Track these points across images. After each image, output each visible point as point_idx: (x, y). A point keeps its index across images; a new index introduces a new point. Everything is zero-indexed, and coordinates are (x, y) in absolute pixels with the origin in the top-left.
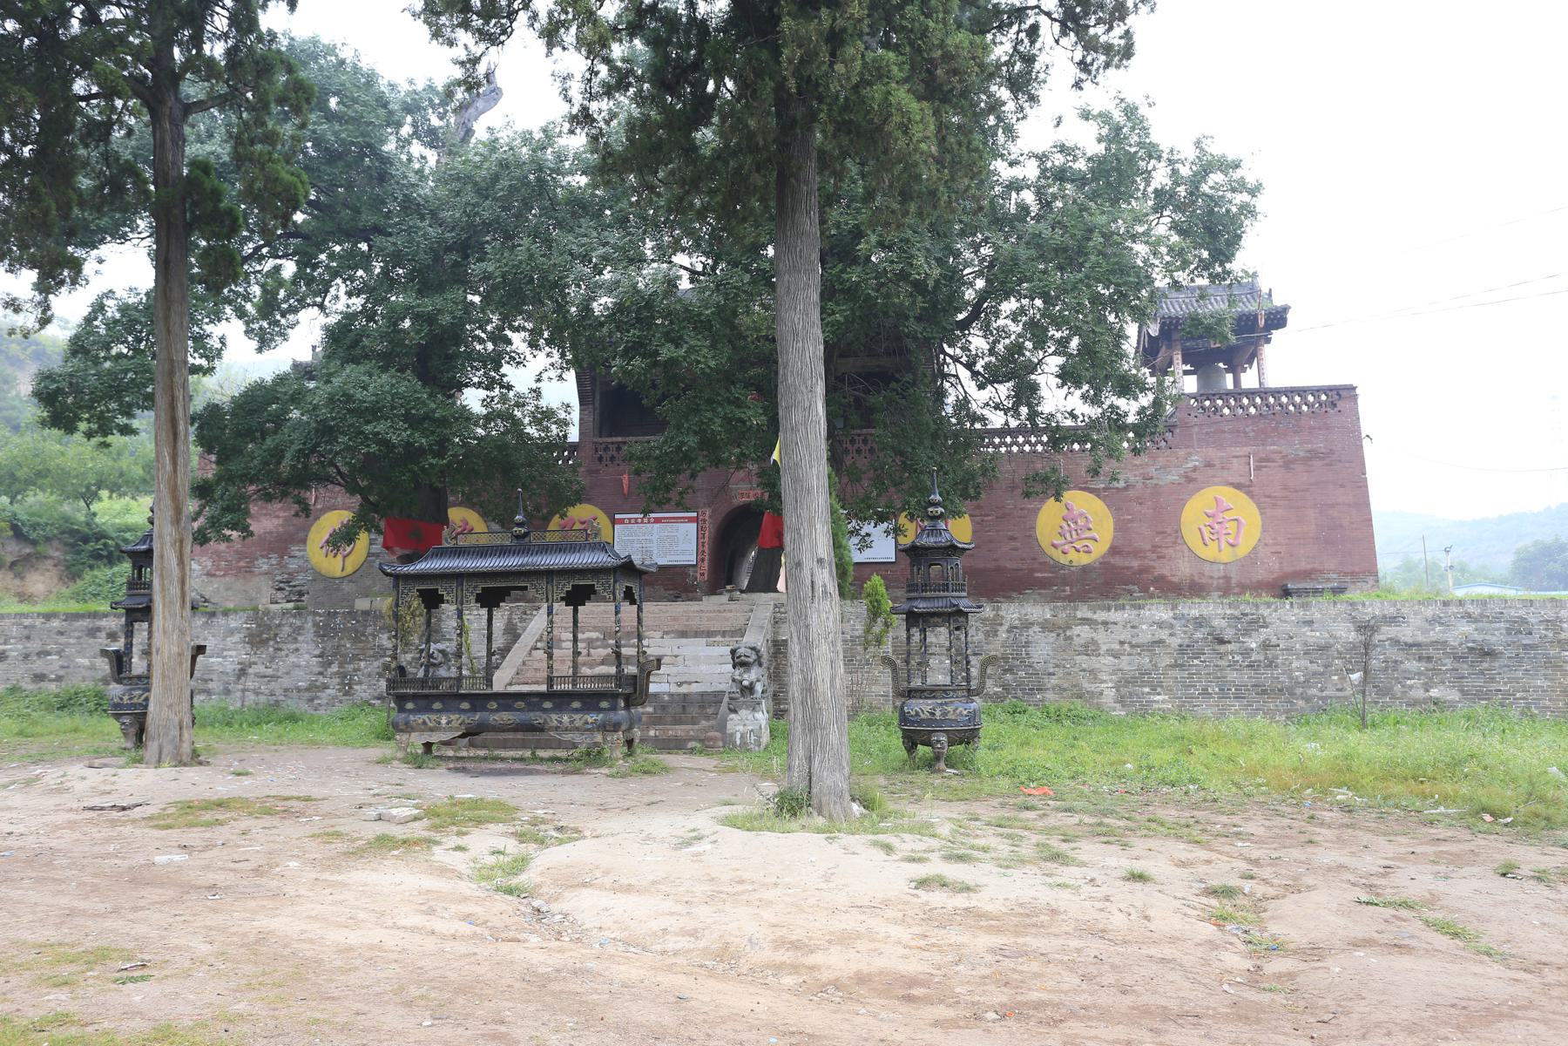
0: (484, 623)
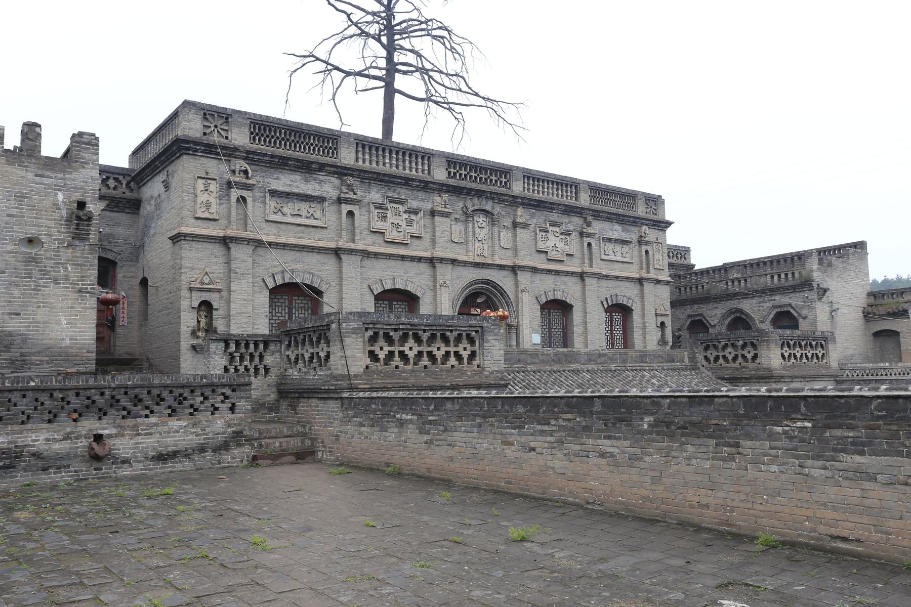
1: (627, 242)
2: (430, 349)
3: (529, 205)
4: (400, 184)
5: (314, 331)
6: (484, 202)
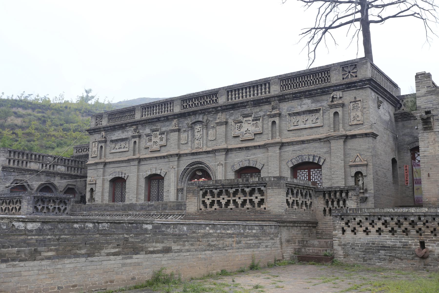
1: (316, 110)
2: (218, 199)
3: (227, 109)
4: (156, 121)
5: (295, 188)
6: (197, 117)
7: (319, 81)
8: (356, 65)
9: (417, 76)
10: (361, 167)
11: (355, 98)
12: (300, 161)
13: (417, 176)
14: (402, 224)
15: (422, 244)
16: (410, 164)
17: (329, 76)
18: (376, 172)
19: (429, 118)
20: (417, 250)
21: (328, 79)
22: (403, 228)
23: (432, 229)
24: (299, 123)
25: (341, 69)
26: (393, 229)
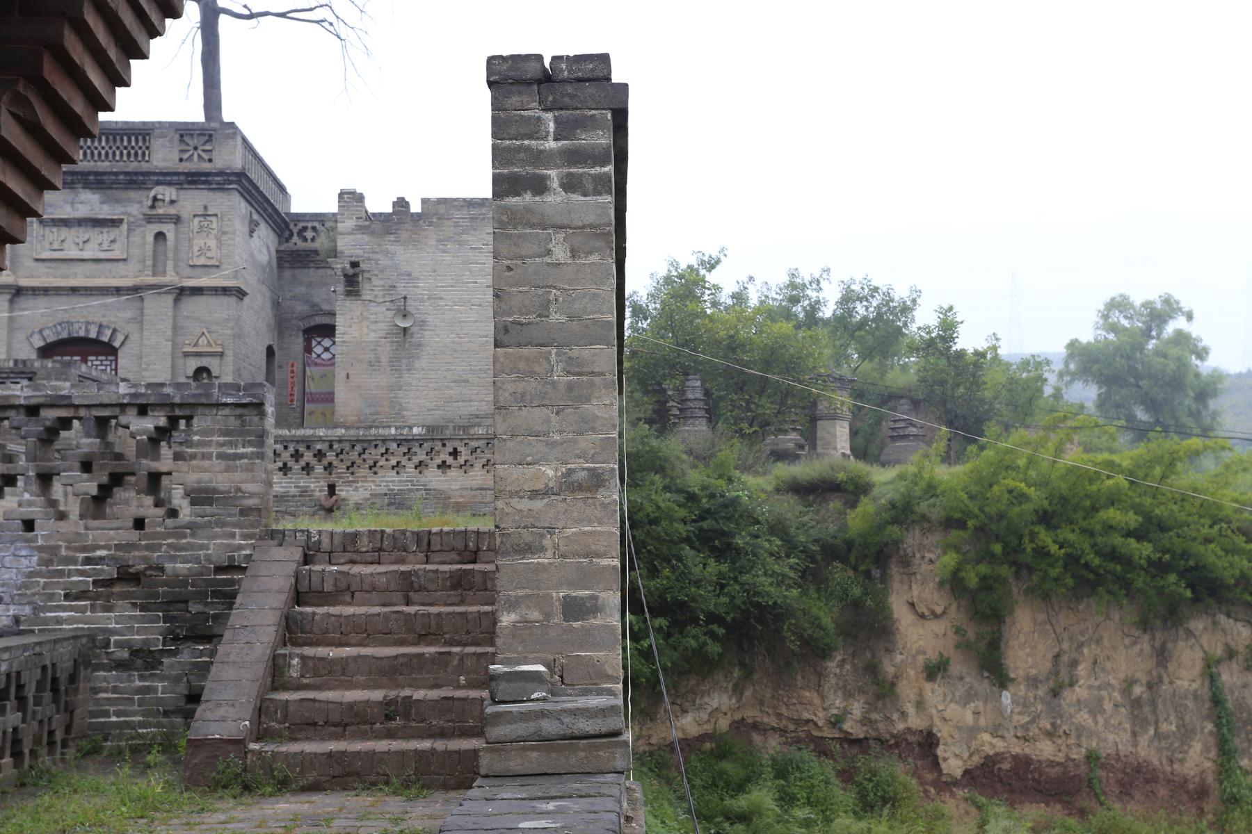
0: (106, 401)
1: (113, 221)
7: (121, 154)
8: (210, 136)
9: (341, 195)
10: (209, 359)
11: (205, 208)
12: (64, 335)
13: (312, 386)
14: (302, 456)
15: (332, 489)
16: (301, 361)
17: (148, 148)
18: (239, 370)
19: (356, 275)
20: (323, 498)
21: (144, 154)
22: (303, 463)
23: (349, 464)
24: (66, 245)
25: (177, 137)
26: (285, 464)
